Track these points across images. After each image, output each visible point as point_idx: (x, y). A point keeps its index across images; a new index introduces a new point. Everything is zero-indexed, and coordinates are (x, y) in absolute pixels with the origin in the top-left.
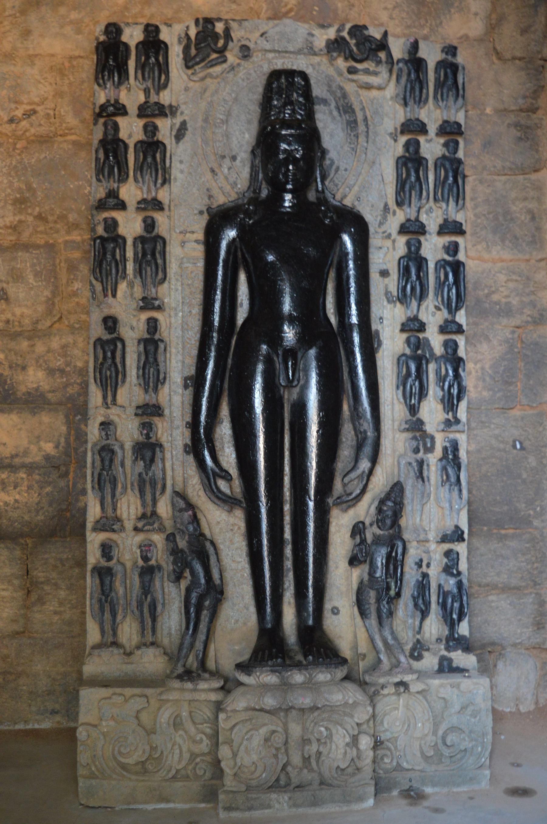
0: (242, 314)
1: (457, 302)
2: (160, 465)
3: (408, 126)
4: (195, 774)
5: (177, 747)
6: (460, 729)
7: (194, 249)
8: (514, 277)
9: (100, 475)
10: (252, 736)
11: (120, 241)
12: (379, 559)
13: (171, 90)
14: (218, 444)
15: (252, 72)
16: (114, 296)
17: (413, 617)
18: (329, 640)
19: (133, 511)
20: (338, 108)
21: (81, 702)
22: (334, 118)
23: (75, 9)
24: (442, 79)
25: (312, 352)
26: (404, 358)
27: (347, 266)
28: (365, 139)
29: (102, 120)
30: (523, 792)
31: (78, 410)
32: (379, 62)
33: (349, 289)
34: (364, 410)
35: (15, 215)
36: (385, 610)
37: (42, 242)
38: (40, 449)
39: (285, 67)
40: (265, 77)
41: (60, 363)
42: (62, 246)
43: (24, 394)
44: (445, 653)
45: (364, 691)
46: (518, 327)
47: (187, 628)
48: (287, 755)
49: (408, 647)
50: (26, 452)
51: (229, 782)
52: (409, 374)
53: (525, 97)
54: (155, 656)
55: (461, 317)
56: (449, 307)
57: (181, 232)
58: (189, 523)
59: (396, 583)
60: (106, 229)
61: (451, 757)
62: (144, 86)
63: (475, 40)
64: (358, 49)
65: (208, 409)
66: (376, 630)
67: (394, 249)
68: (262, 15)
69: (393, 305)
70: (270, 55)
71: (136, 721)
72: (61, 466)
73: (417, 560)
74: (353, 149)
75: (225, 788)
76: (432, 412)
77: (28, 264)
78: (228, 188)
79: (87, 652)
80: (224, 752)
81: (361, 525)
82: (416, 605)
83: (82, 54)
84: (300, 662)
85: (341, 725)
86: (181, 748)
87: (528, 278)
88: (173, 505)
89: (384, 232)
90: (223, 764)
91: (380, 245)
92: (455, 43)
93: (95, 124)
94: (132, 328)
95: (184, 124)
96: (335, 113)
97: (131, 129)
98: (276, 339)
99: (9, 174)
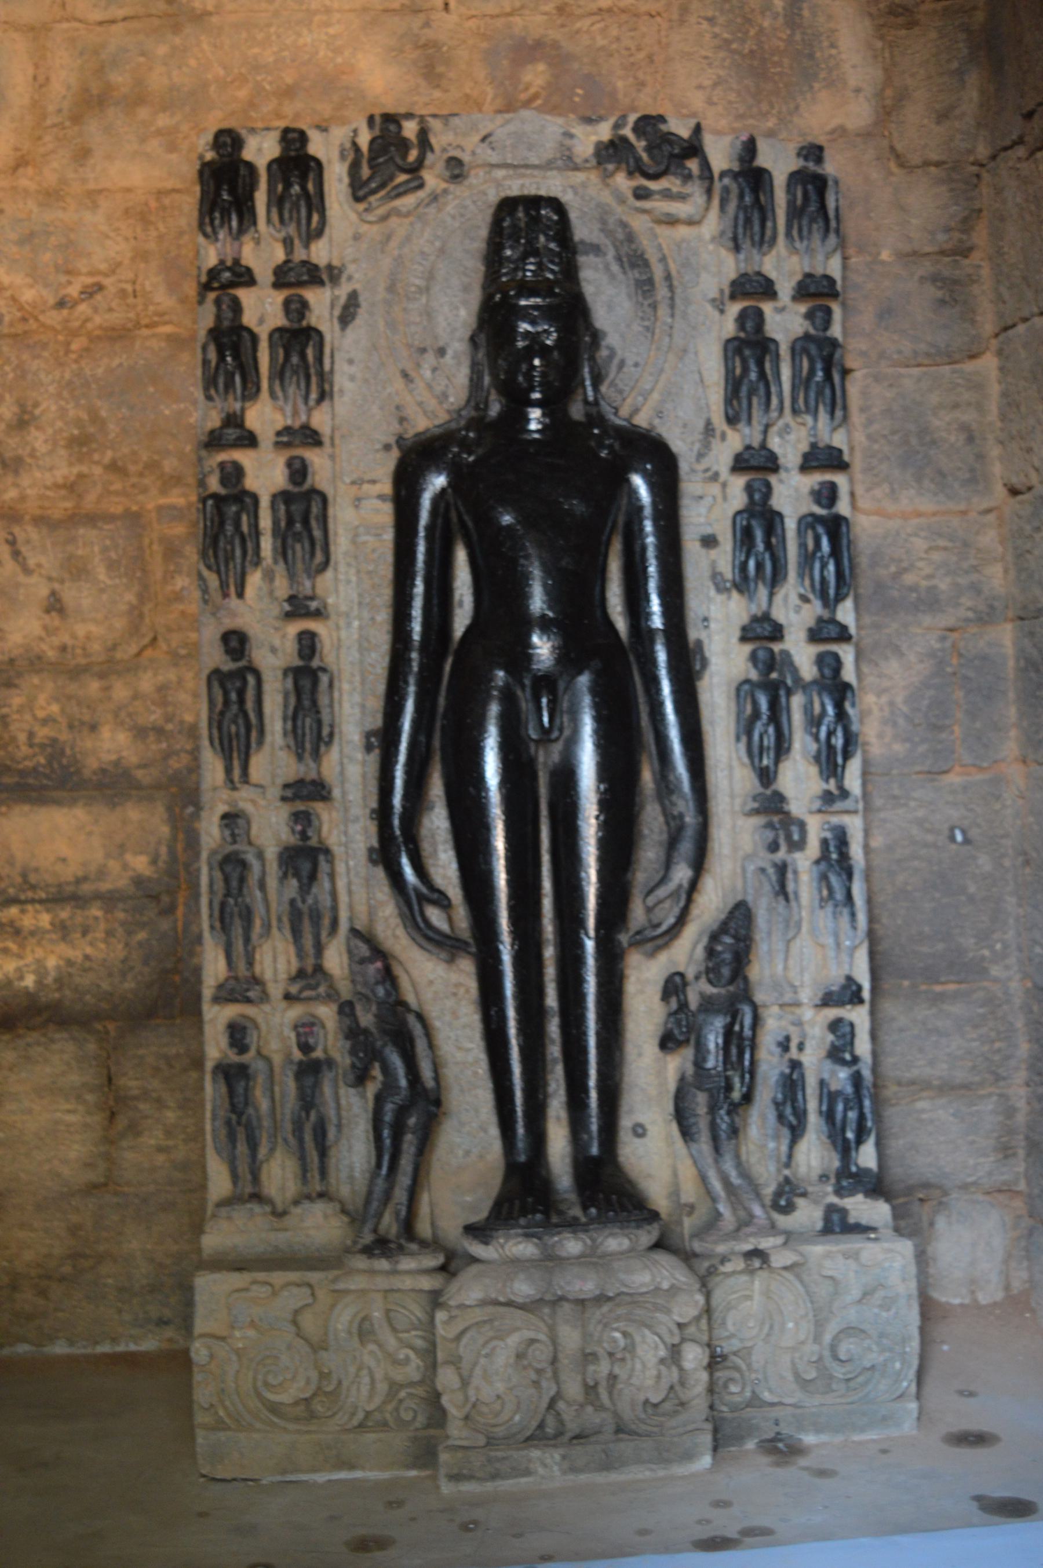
0: (462, 620)
1: (838, 587)
2: (327, 885)
3: (742, 284)
4: (399, 1420)
5: (365, 1372)
6: (863, 1331)
7: (377, 511)
8: (941, 543)
9: (223, 905)
10: (494, 1349)
11: (248, 500)
12: (711, 1037)
13: (331, 241)
14: (426, 847)
15: (468, 202)
16: (241, 595)
17: (777, 1137)
18: (630, 1182)
19: (282, 966)
20: (619, 259)
21: (197, 1298)
22: (613, 277)
23: (164, 109)
24: (799, 202)
25: (584, 680)
26: (746, 687)
27: (642, 529)
28: (669, 311)
29: (212, 296)
30: (977, 1439)
31: (183, 796)
32: (688, 177)
33: (645, 568)
34: (678, 779)
35: (71, 464)
36: (724, 1126)
37: (119, 510)
38: (125, 866)
39: (526, 192)
40: (490, 211)
41: (155, 716)
42: (154, 515)
43: (95, 773)
44: (834, 1199)
45: (691, 1268)
46: (951, 630)
47: (379, 1165)
48: (558, 1383)
49: (769, 1191)
50: (102, 873)
51: (456, 1431)
52: (756, 715)
53: (948, 230)
54: (326, 1216)
55: (846, 613)
56: (823, 595)
57: (353, 483)
58: (377, 983)
59: (742, 1077)
60: (224, 481)
61: (848, 1380)
62: (283, 234)
63: (858, 135)
64: (651, 156)
65: (407, 784)
66: (710, 1161)
67: (725, 498)
68: (487, 107)
69: (724, 597)
70: (500, 173)
71: (293, 1329)
72: (158, 896)
73: (780, 1038)
74: (647, 328)
75: (450, 1442)
76: (799, 779)
77: (96, 549)
78: (432, 404)
79: (209, 1212)
80: (447, 1378)
81: (678, 979)
82: (781, 1117)
83: (179, 186)
84: (576, 1219)
85: (649, 1327)
86: (372, 1374)
87: (966, 544)
88: (350, 952)
89: (707, 470)
90: (445, 1400)
91: (699, 493)
92: (821, 140)
93: (201, 301)
94: (273, 650)
95: (353, 296)
96: (615, 268)
97: (262, 309)
98: (519, 657)
99: (59, 396)
